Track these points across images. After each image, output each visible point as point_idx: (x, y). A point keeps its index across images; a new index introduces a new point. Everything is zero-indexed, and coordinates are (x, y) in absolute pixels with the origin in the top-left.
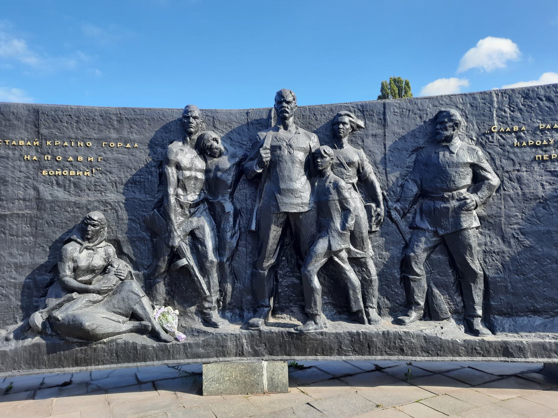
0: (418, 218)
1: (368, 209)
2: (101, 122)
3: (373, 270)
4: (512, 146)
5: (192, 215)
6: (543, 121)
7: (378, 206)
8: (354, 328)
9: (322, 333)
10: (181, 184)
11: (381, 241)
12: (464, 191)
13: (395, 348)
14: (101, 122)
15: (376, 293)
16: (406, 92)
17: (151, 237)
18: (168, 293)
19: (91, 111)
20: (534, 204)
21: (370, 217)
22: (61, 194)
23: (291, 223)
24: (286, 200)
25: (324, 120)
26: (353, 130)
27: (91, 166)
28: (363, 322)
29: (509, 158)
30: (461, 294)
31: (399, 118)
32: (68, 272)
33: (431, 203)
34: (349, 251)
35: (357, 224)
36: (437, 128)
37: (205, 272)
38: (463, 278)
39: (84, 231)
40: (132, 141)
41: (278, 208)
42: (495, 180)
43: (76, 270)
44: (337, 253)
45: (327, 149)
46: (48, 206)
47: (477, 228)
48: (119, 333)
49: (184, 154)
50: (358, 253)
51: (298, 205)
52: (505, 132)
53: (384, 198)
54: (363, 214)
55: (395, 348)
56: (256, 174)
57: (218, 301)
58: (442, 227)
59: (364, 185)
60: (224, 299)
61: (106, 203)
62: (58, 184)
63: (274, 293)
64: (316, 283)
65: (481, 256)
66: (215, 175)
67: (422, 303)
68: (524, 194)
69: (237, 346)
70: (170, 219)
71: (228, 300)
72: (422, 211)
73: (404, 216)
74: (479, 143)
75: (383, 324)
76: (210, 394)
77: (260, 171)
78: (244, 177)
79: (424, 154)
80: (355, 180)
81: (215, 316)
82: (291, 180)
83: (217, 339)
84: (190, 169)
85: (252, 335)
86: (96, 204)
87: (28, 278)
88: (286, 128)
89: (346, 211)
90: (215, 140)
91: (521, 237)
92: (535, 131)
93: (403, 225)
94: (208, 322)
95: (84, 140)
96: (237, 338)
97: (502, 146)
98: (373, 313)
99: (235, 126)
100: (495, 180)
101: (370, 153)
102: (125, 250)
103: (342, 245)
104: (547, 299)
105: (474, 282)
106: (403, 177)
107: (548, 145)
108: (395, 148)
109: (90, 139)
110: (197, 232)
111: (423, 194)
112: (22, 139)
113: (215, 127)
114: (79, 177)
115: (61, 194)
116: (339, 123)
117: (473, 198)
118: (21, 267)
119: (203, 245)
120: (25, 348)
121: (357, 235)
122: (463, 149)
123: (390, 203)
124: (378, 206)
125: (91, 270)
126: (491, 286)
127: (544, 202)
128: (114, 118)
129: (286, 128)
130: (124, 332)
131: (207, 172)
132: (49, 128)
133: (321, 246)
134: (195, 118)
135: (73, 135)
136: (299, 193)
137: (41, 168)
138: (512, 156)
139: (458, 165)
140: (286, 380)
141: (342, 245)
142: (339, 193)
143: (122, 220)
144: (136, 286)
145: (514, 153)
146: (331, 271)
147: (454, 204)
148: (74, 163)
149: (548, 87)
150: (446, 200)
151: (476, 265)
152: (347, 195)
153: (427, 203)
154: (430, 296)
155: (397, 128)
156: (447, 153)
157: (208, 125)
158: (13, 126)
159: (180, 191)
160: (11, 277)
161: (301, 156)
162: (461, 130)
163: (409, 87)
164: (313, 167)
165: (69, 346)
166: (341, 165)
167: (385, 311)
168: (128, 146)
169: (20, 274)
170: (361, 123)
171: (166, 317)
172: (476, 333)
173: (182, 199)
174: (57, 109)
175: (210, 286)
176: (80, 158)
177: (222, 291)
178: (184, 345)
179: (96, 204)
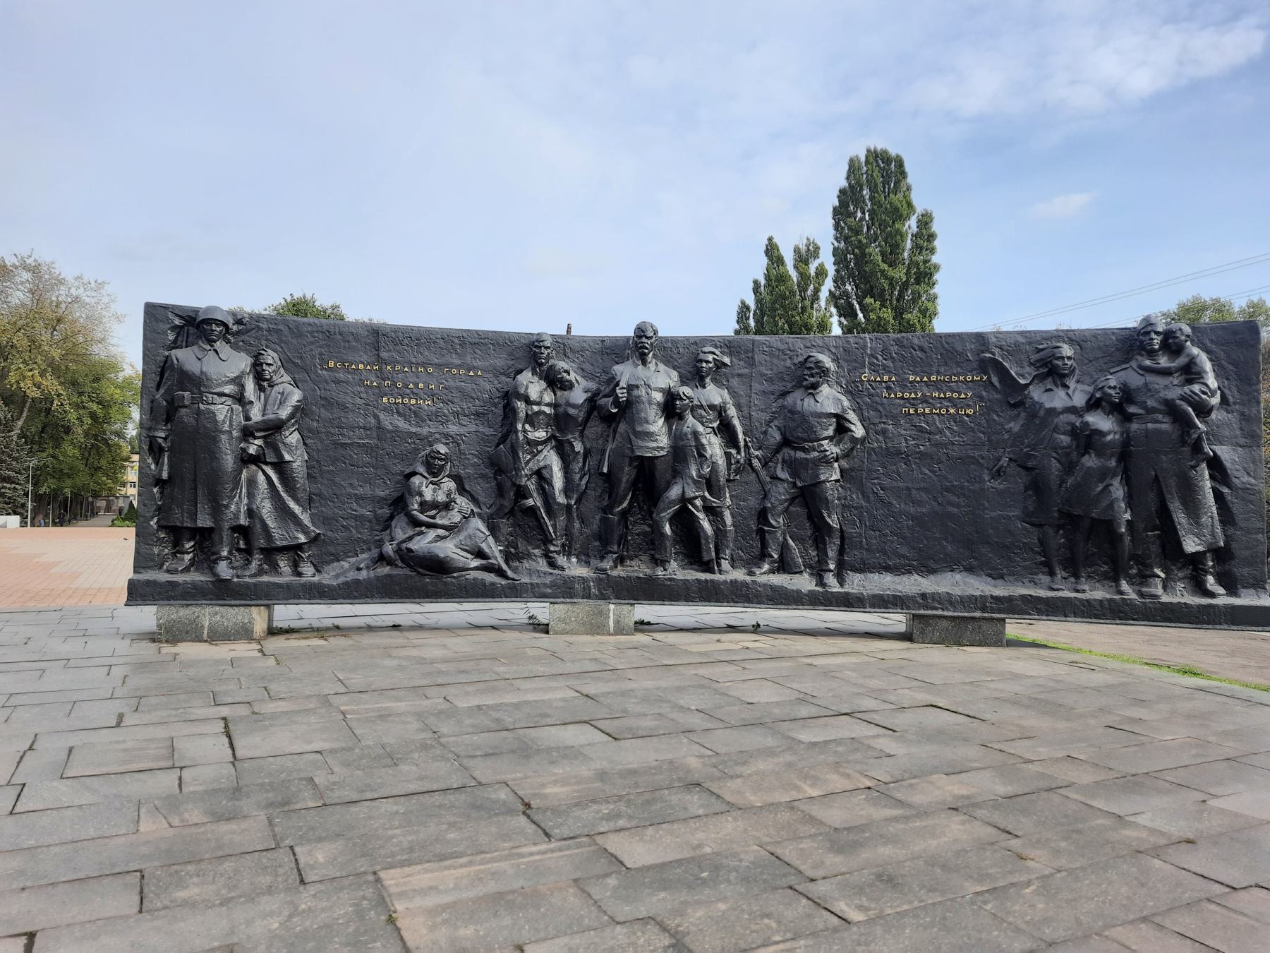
1: (728, 455)
2: (443, 345)
6: (915, 374)
7: (739, 453)
9: (670, 579)
10: (530, 419)
14: (443, 345)
17: (495, 474)
19: (429, 331)
21: (729, 464)
22: (401, 424)
23: (645, 467)
24: (641, 443)
26: (718, 368)
28: (713, 572)
30: (817, 548)
32: (416, 506)
33: (792, 453)
34: (704, 498)
35: (714, 470)
38: (820, 532)
42: (858, 431)
44: (691, 501)
47: (837, 481)
50: (715, 502)
51: (654, 449)
53: (746, 445)
54: (721, 462)
55: (742, 596)
56: (611, 412)
58: (800, 478)
59: (726, 430)
61: (447, 436)
62: (398, 413)
63: (623, 540)
64: (667, 529)
65: (839, 510)
72: (784, 461)
74: (848, 392)
77: (615, 411)
78: (595, 413)
79: (790, 400)
81: (561, 560)
82: (647, 422)
84: (539, 404)
88: (644, 363)
92: (903, 384)
93: (763, 473)
94: (552, 564)
95: (425, 365)
100: (858, 431)
101: (733, 394)
104: (900, 556)
110: (544, 472)
111: (786, 442)
113: (812, 880)
115: (401, 424)
116: (701, 361)
117: (833, 449)
118: (362, 499)
119: (550, 484)
120: (377, 578)
121: (714, 483)
123: (752, 450)
124: (739, 453)
125: (435, 505)
126: (847, 541)
128: (456, 341)
133: (675, 492)
135: (414, 360)
136: (657, 435)
138: (880, 408)
144: (478, 524)
145: (882, 404)
146: (684, 519)
151: (833, 521)
152: (704, 441)
153: (787, 452)
156: (812, 401)
157: (558, 353)
159: (527, 427)
161: (658, 397)
164: (672, 408)
170: (727, 360)
176: (421, 386)
179: (437, 436)
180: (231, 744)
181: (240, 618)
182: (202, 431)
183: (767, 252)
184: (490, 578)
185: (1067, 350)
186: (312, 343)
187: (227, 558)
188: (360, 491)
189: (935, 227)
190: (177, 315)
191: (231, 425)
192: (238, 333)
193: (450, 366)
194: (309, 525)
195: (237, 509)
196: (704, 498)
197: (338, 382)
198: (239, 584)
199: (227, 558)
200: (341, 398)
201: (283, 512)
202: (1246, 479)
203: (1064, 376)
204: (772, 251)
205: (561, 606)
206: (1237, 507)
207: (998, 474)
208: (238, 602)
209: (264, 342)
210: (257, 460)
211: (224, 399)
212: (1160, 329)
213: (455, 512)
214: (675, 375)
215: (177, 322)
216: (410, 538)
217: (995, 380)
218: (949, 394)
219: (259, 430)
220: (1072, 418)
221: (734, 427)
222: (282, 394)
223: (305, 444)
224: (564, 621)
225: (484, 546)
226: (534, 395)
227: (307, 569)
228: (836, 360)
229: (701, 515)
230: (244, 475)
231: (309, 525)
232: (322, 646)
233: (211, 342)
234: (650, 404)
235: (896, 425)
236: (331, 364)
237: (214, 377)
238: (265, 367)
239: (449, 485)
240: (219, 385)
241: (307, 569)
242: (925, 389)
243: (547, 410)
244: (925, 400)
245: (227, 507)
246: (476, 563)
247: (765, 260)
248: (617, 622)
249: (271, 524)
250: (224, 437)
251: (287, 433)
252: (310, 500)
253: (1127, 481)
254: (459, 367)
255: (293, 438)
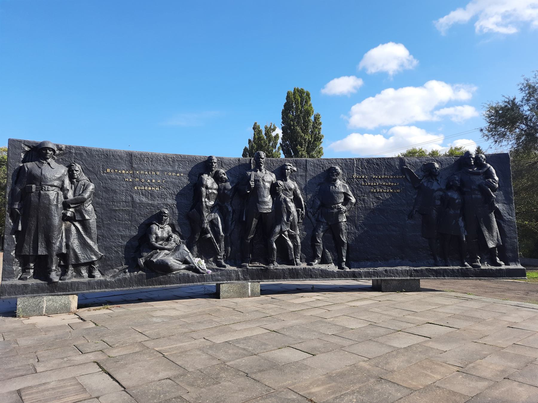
0: (320, 216)
1: (298, 211)
2: (164, 161)
3: (299, 241)
4: (361, 185)
5: (212, 212)
7: (302, 210)
8: (290, 267)
9: (276, 269)
10: (208, 197)
11: (303, 227)
12: (340, 205)
13: (308, 275)
14: (164, 161)
15: (300, 252)
16: (306, 102)
18: (198, 251)
20: (369, 211)
22: (144, 199)
23: (262, 217)
24: (261, 206)
25: (277, 166)
27: (159, 185)
29: (360, 190)
31: (313, 168)
32: (154, 240)
34: (288, 231)
35: (293, 219)
36: (329, 175)
37: (219, 241)
39: (159, 218)
40: (180, 173)
41: (258, 210)
42: (353, 200)
43: (157, 238)
45: (280, 182)
46: (138, 205)
48: (180, 270)
49: (209, 180)
51: (267, 209)
52: (359, 178)
54: (295, 214)
55: (308, 275)
57: (224, 256)
60: (227, 254)
61: (167, 205)
66: (224, 192)
67: (320, 256)
68: (365, 207)
69: (236, 275)
70: (203, 214)
71: (229, 255)
73: (313, 215)
74: (347, 183)
75: (304, 265)
76: (224, 298)
80: (292, 197)
82: (264, 197)
83: (227, 272)
84: (211, 189)
85: (244, 271)
86: (162, 205)
87: (127, 243)
88: (261, 170)
89: (289, 213)
90: (223, 174)
91: (363, 226)
92: (371, 179)
93: (313, 220)
96: (237, 272)
97: (357, 184)
98: (298, 261)
99: (233, 166)
100: (353, 200)
102: (177, 229)
103: (286, 228)
105: (343, 246)
106: (313, 196)
107: (376, 185)
108: (310, 182)
109: (158, 171)
110: (214, 221)
111: (323, 205)
112: (124, 170)
114: (153, 191)
115: (144, 199)
117: (344, 208)
122: (340, 185)
123: (308, 209)
124: (302, 210)
125: (162, 239)
127: (373, 211)
129: (261, 170)
130: (182, 269)
131: (218, 190)
132: (138, 164)
134: (215, 163)
135: (150, 169)
137: (134, 185)
138: (361, 189)
139: (338, 193)
140: (259, 291)
141: (286, 228)
142: (287, 204)
143: (176, 213)
145: (362, 188)
146: (281, 242)
147: (336, 210)
148: (151, 183)
149: (378, 159)
150: (333, 209)
151: (344, 239)
154: (324, 253)
155: (312, 173)
156: (334, 187)
158: (119, 163)
159: (206, 200)
160: (119, 242)
161: (268, 185)
162: (340, 176)
163: (309, 98)
164: (274, 189)
165: (157, 275)
166: (286, 190)
167: (304, 260)
168: (178, 175)
169: (124, 240)
170: (295, 169)
171: (200, 263)
172: (343, 268)
173: (208, 204)
174: (141, 154)
175: (221, 247)
176: (154, 181)
177: (226, 251)
178: (211, 275)
179: (162, 205)
180: (112, 377)
181: (63, 301)
182: (42, 204)
183: (254, 128)
184: (191, 273)
185: (437, 165)
186: (98, 160)
187: (55, 270)
188: (123, 233)
189: (321, 120)
190: (26, 145)
191: (57, 201)
192: (59, 155)
193: (168, 171)
194: (98, 251)
195: (59, 243)
196: (288, 231)
197: (112, 179)
198: (62, 284)
199: (55, 270)
200: (114, 187)
201: (84, 244)
202: (509, 217)
203: (437, 175)
204: (256, 128)
205: (226, 285)
206: (506, 229)
207: (411, 216)
208: (62, 293)
209: (73, 160)
210: (72, 219)
211: (54, 188)
212: (474, 157)
213: (172, 242)
214: (274, 175)
215: (27, 149)
216: (152, 256)
217: (408, 177)
218: (390, 183)
219: (72, 204)
220: (441, 193)
221: (300, 198)
222: (84, 185)
223: (95, 210)
224: (227, 292)
225: (187, 257)
226: (209, 185)
227: (98, 275)
228: (342, 169)
229: (288, 239)
230: (63, 227)
231: (98, 251)
232: (109, 315)
233: (46, 159)
234: (265, 188)
235: (369, 197)
236: (108, 170)
237: (48, 176)
238: (75, 172)
239: (168, 228)
240: (51, 181)
241: (98, 275)
242: (379, 181)
243: (215, 192)
244: (380, 186)
245: (55, 244)
246: (184, 266)
247: (253, 132)
248: (252, 291)
249: (78, 251)
250: (53, 208)
251: (87, 205)
252: (98, 239)
253: (464, 220)
254: (172, 172)
255: (90, 207)
